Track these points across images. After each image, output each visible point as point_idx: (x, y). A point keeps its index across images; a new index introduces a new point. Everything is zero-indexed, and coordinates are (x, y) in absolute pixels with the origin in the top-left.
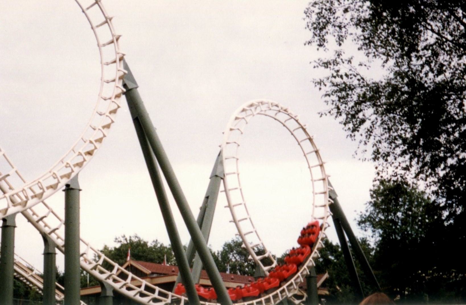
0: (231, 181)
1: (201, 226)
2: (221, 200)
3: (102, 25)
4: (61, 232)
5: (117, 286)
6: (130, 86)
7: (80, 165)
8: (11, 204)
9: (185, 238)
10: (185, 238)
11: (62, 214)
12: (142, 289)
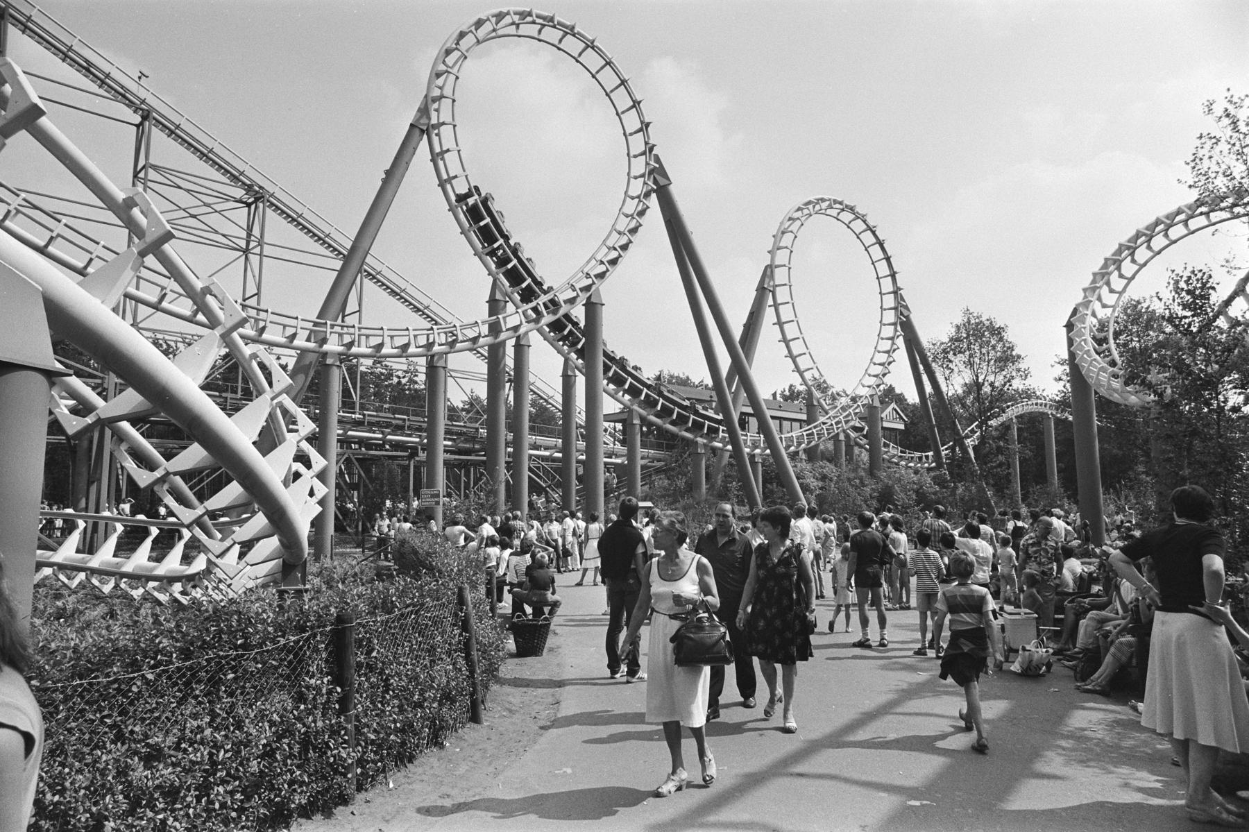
0: (782, 295)
2: (769, 315)
3: (636, 132)
4: (559, 399)
6: (662, 181)
7: (601, 276)
8: (524, 320)
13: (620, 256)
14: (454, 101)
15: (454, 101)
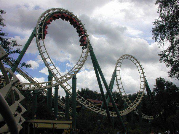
0: (118, 77)
1: (110, 88)
2: (115, 82)
4: (71, 91)
5: (86, 106)
9: (105, 91)
10: (105, 91)
11: (71, 85)
12: (93, 107)
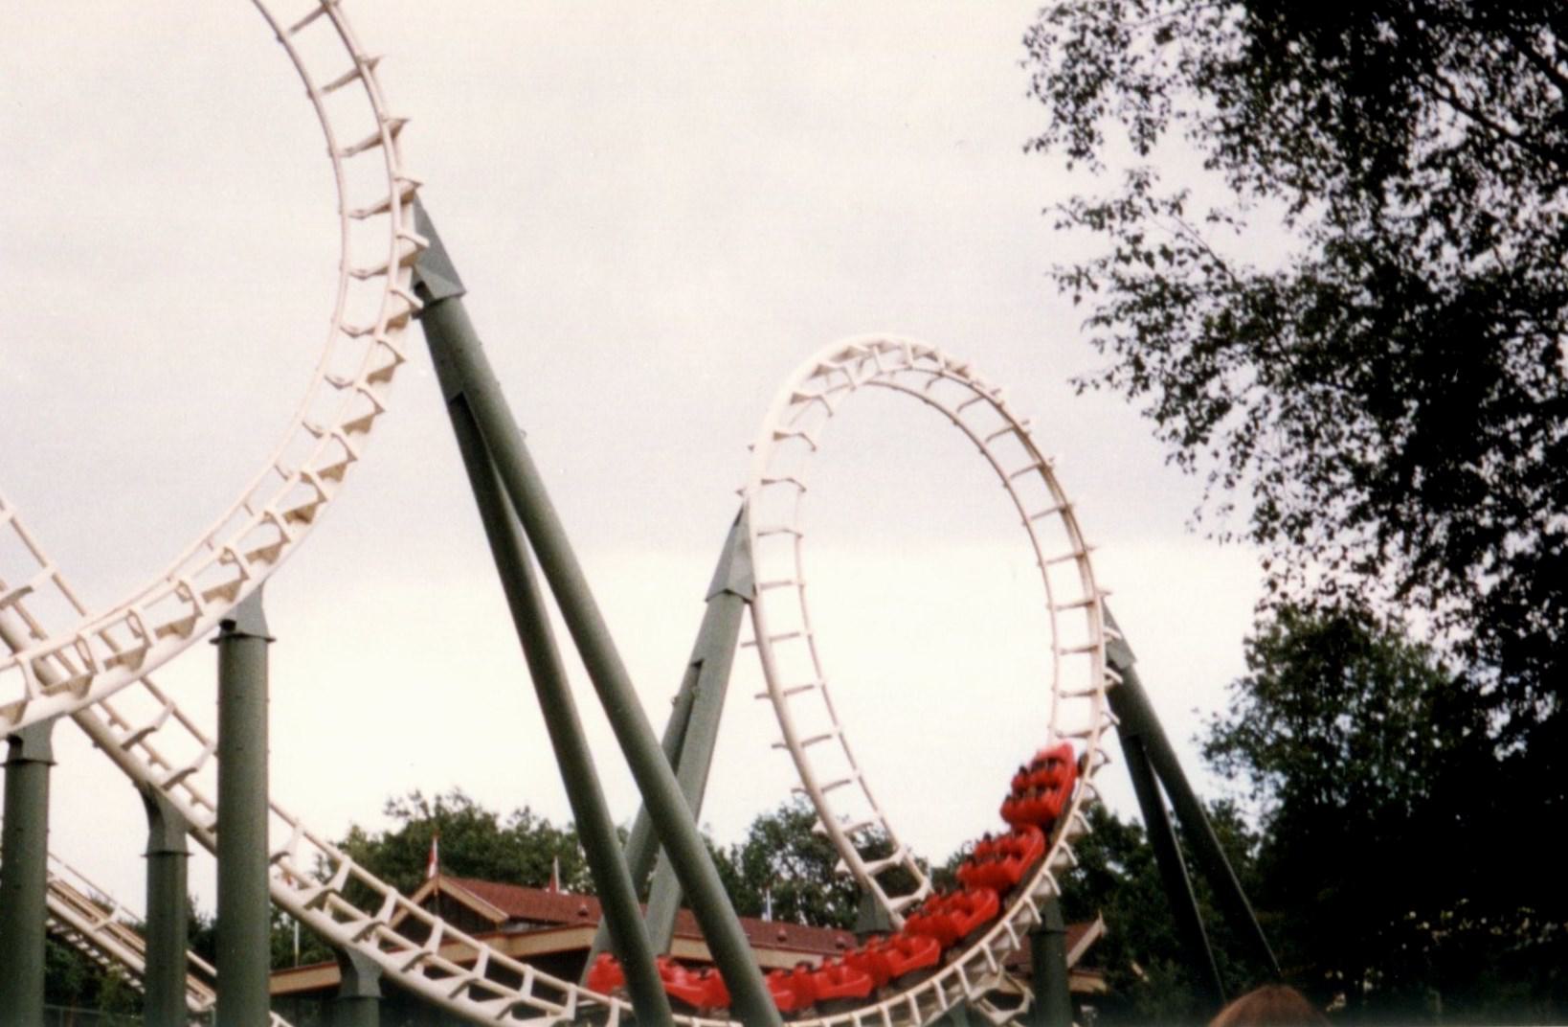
0: (776, 609)
1: (675, 762)
2: (744, 672)
3: (342, 83)
4: (207, 782)
5: (394, 962)
6: (438, 288)
7: (268, 555)
8: (36, 686)
9: (623, 803)
10: (623, 803)
11: (208, 719)
12: (479, 972)
13: (285, 539)
14: (801, 587)
15: (801, 587)
